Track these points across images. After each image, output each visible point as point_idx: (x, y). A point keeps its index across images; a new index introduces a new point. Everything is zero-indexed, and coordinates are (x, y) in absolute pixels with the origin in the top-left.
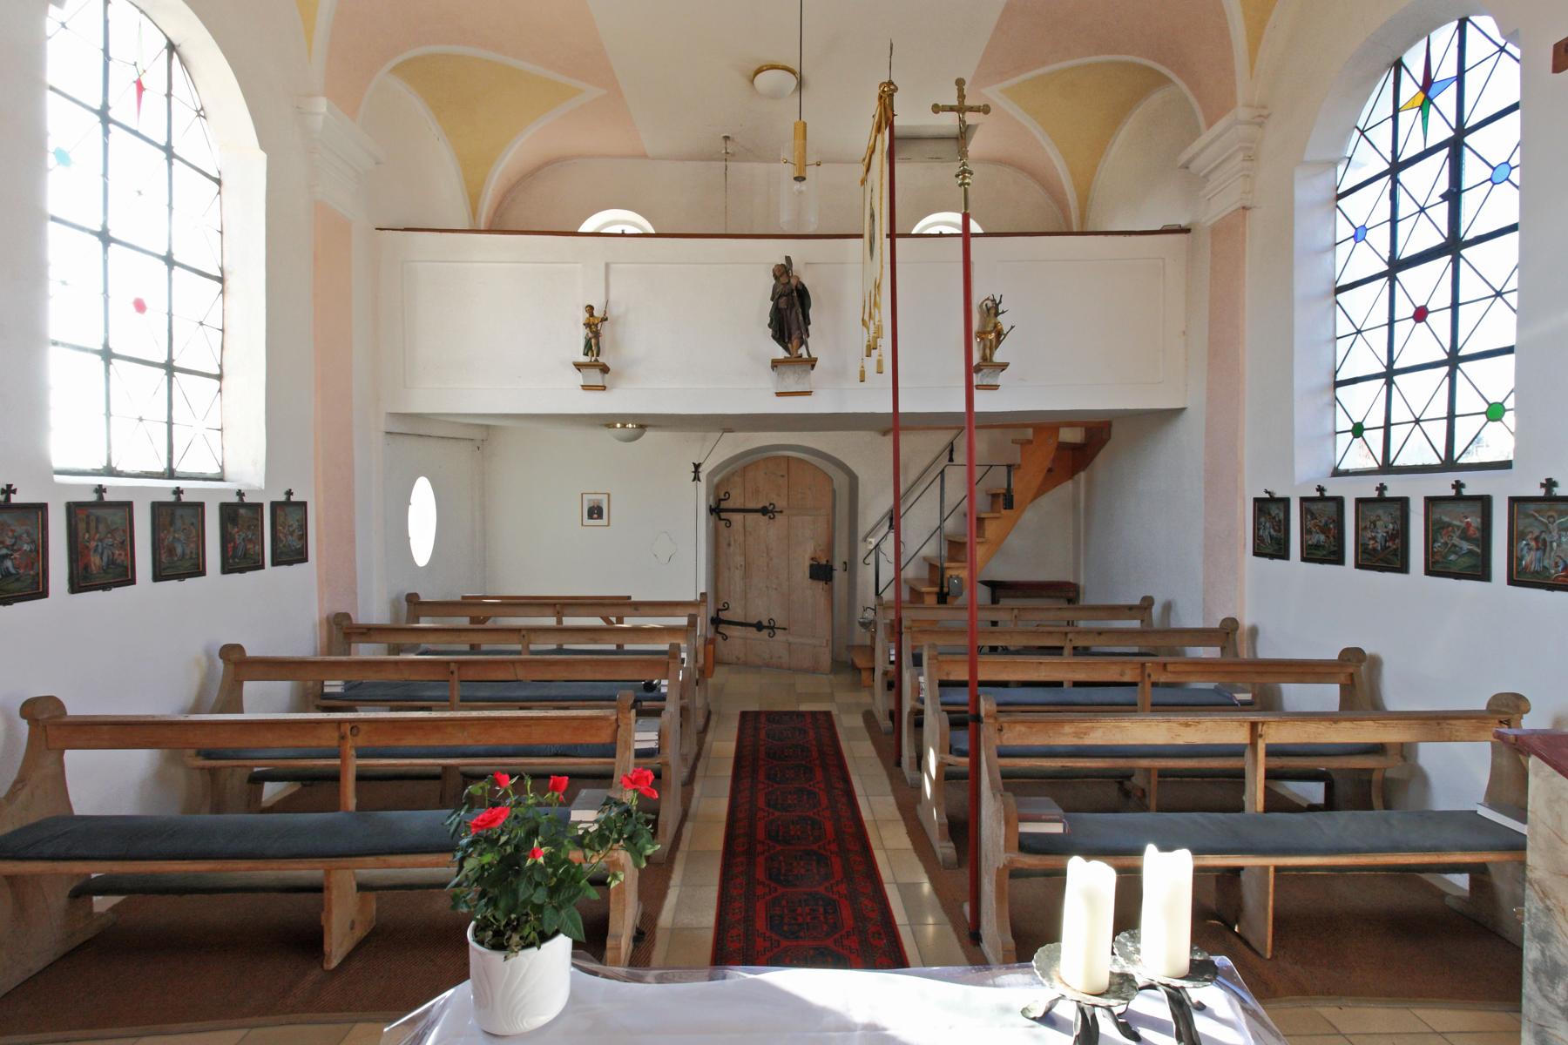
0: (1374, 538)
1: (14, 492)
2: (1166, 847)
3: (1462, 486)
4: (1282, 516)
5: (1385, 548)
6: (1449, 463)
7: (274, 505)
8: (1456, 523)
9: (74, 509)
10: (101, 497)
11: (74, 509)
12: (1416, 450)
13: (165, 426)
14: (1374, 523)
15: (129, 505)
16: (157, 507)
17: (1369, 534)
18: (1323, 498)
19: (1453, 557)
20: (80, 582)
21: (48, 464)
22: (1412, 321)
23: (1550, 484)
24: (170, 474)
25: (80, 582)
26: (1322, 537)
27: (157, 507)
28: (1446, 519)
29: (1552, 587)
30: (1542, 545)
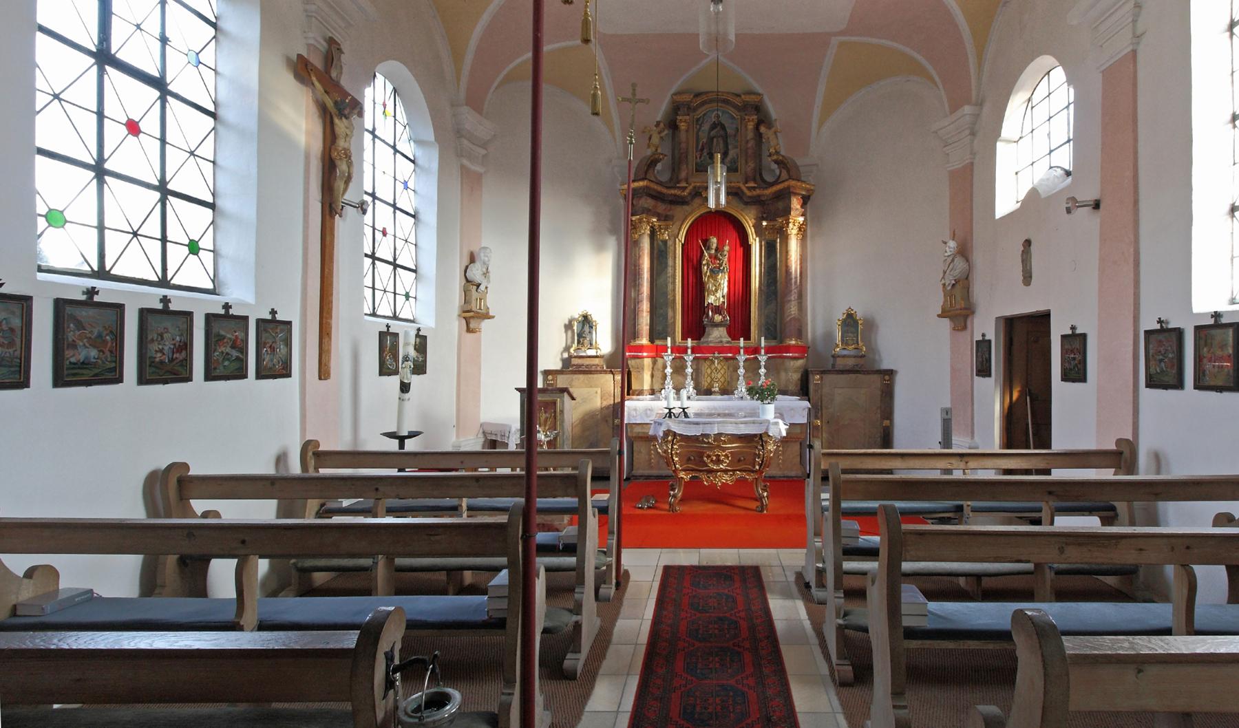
0: (161, 351)
1: (97, 293)
2: (1070, 81)
3: (169, 301)
4: (16, 322)
5: (171, 360)
6: (164, 282)
7: (260, 322)
8: (229, 336)
9: (61, 306)
10: (227, 311)
11: (61, 306)
12: (136, 262)
13: (94, 233)
14: (161, 335)
15: (120, 308)
16: (144, 313)
17: (155, 346)
18: (274, 321)
19: (226, 363)
20: (64, 376)
21: (34, 253)
22: (124, 120)
23: (273, 312)
24: (164, 282)
25: (64, 376)
26: (93, 353)
27: (144, 313)
28: (222, 333)
29: (275, 377)
30: (273, 349)
